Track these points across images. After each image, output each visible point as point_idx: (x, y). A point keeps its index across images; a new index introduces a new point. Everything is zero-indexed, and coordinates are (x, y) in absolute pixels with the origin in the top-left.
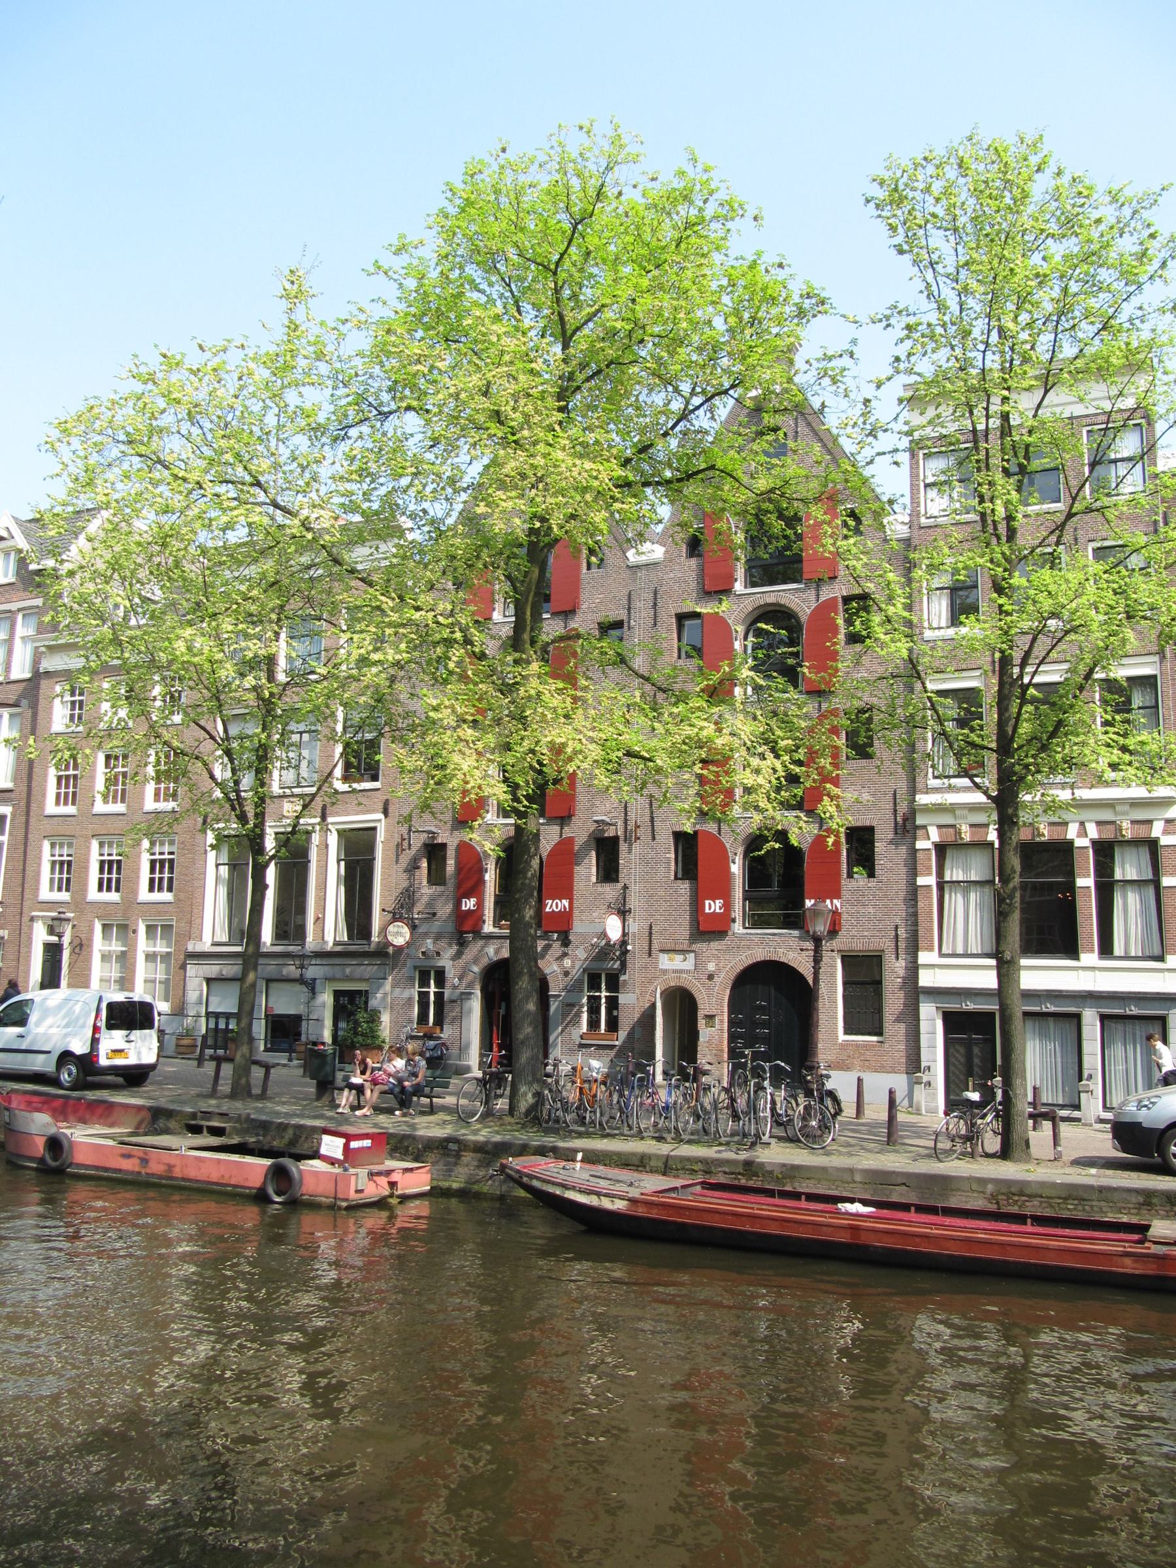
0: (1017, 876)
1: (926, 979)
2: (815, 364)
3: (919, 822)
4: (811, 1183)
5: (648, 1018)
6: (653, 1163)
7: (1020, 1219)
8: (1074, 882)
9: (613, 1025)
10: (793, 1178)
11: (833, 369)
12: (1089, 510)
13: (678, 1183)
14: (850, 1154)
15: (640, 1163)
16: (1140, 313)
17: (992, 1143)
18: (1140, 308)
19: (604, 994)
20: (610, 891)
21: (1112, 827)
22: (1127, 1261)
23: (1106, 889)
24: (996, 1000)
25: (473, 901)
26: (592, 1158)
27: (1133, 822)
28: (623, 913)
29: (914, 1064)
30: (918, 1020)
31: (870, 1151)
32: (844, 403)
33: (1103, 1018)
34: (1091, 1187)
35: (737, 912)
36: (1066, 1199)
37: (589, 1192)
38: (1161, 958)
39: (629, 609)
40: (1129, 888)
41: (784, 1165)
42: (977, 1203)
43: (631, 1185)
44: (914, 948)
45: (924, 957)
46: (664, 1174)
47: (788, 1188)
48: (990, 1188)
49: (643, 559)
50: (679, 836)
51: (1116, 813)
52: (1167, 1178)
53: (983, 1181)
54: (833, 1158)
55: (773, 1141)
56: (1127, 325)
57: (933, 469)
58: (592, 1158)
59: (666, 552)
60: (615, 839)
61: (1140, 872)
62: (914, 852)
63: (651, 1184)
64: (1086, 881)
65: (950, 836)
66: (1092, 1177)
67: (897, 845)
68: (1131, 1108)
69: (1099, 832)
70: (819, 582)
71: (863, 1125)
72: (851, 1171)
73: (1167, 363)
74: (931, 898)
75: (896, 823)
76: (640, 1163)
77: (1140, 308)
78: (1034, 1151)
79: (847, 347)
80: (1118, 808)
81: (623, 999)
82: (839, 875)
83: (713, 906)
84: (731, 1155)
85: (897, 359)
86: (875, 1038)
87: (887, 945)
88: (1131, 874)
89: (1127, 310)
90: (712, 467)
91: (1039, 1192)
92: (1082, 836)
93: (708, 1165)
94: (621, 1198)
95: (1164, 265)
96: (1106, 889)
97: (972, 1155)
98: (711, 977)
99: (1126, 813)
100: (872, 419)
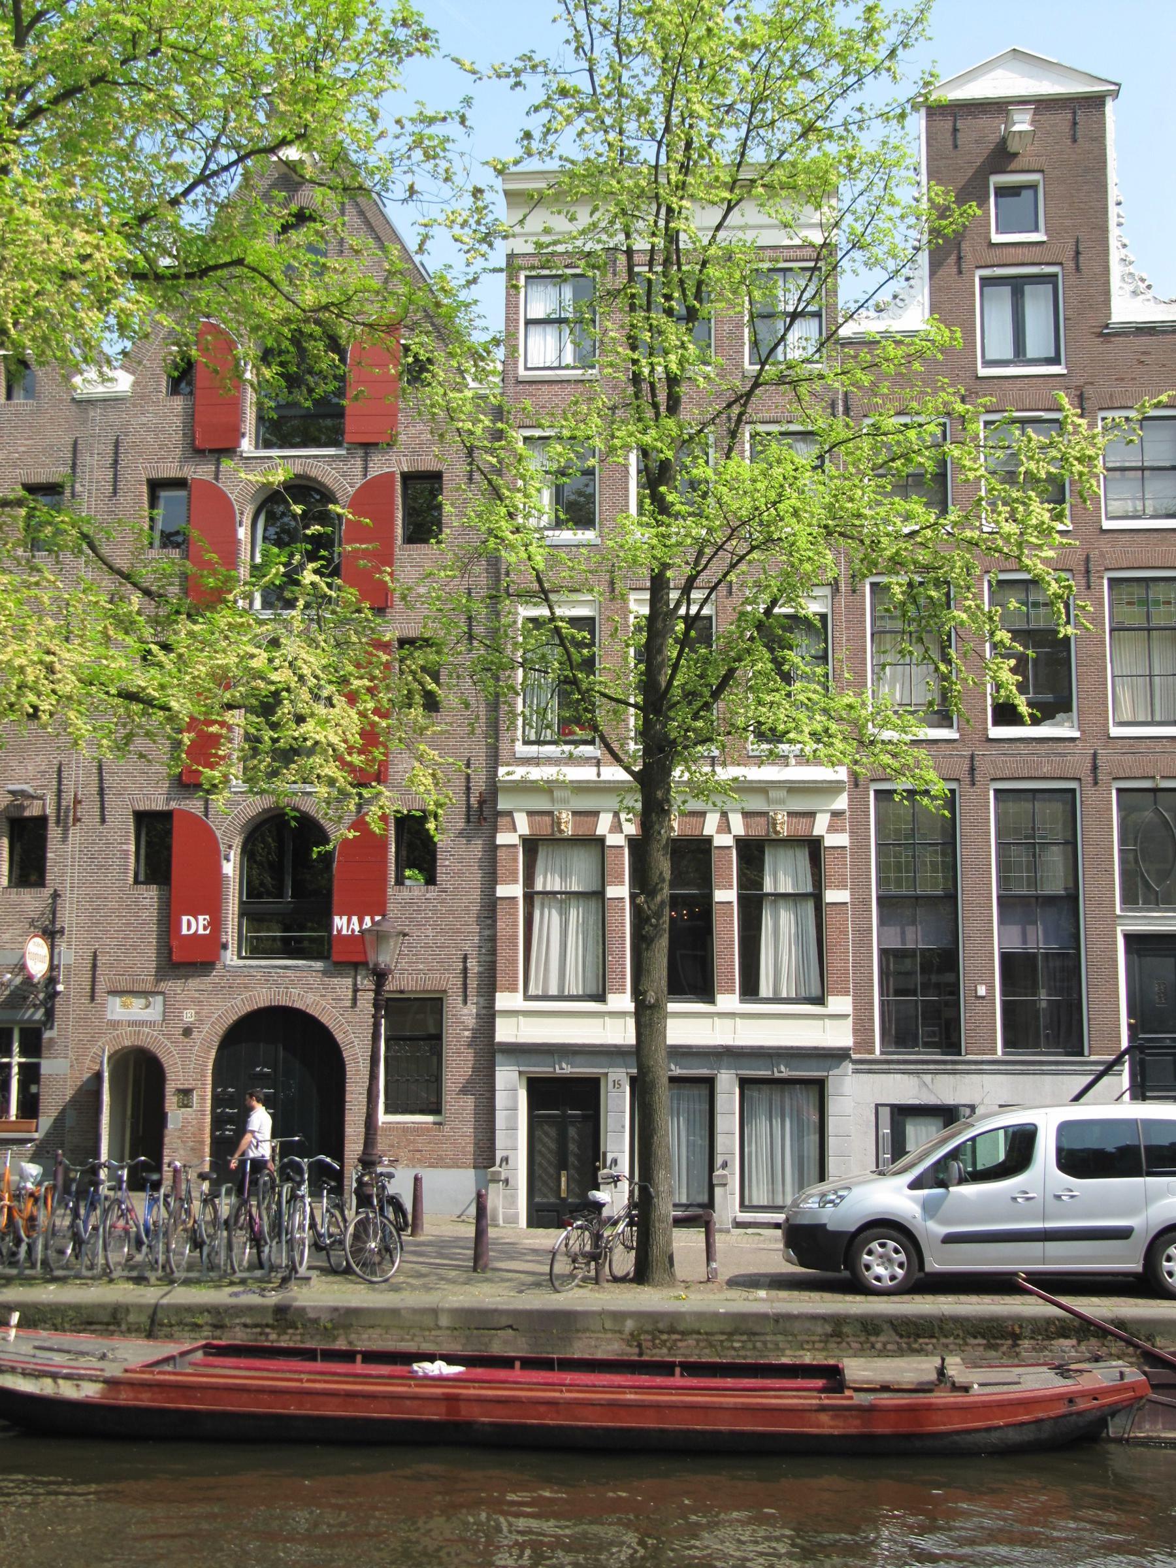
0: (666, 886)
1: (505, 1032)
2: (409, 127)
3: (501, 806)
4: (375, 1333)
5: (88, 1096)
6: (132, 1318)
7: (666, 1368)
8: (710, 896)
9: (30, 1107)
10: (347, 1327)
11: (430, 138)
12: (781, 380)
13: (171, 1349)
14: (428, 1289)
15: (109, 1321)
16: (857, 116)
17: (623, 1261)
18: (860, 110)
19: (16, 1060)
20: (32, 900)
21: (763, 820)
22: (824, 1418)
23: (752, 906)
24: (633, 1060)
25: (203, 919)
26: (33, 1318)
27: (790, 814)
28: (51, 934)
29: (485, 1155)
30: (492, 1090)
31: (453, 1282)
32: (446, 190)
33: (744, 1083)
34: (764, 1316)
35: (230, 934)
36: (731, 1334)
37: (38, 1375)
38: (820, 1001)
39: (74, 466)
40: (781, 903)
41: (336, 1309)
42: (609, 1348)
43: (103, 1357)
44: (489, 988)
45: (503, 1000)
46: (150, 1335)
47: (341, 1344)
48: (630, 1324)
49: (99, 390)
50: (143, 819)
51: (553, 801)
52: (858, 1298)
53: (619, 1316)
54: (405, 1294)
55: (314, 1274)
56: (840, 131)
57: (540, 303)
58: (33, 1318)
59: (135, 384)
60: (42, 820)
61: (796, 883)
62: (492, 848)
63: (132, 1354)
64: (726, 895)
65: (544, 827)
66: (762, 1301)
67: (469, 839)
68: (812, 1204)
69: (747, 826)
70: (368, 447)
71: (423, 1244)
72: (435, 1312)
73: (895, 191)
74: (516, 915)
75: (469, 806)
76: (109, 1321)
77: (860, 110)
78: (680, 1271)
79: (455, 106)
80: (773, 794)
81: (48, 1066)
82: (385, 880)
83: (194, 925)
84: (254, 1299)
85: (528, 135)
86: (430, 1119)
87: (452, 982)
88: (786, 886)
89: (843, 109)
90: (240, 262)
91: (696, 1326)
92: (723, 831)
93: (219, 1316)
94: (92, 1379)
95: (892, 54)
96: (752, 906)
97: (597, 1280)
98: (187, 1032)
99: (782, 802)
100: (489, 219)
